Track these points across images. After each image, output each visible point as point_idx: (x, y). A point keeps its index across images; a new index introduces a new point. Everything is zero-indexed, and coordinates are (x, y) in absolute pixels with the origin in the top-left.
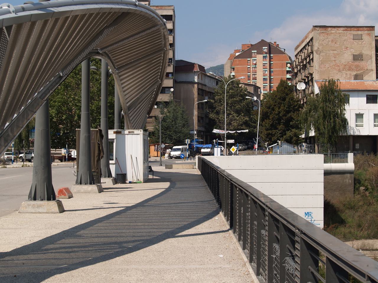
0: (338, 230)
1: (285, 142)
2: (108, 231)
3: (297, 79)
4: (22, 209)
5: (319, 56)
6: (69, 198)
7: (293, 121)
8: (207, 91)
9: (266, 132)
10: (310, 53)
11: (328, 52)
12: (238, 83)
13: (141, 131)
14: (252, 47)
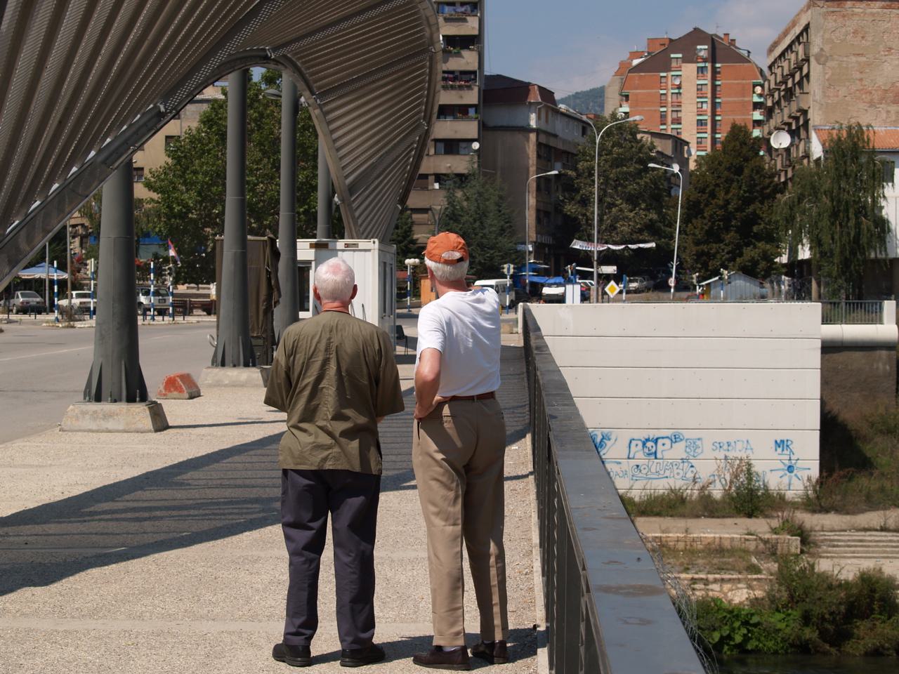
0: (853, 484)
1: (741, 273)
2: (250, 473)
3: (773, 123)
4: (67, 423)
5: (824, 69)
6: (191, 398)
7: (760, 224)
8: (559, 150)
9: (694, 249)
10: (803, 60)
11: (845, 59)
12: (634, 130)
13: (374, 242)
14: (673, 45)
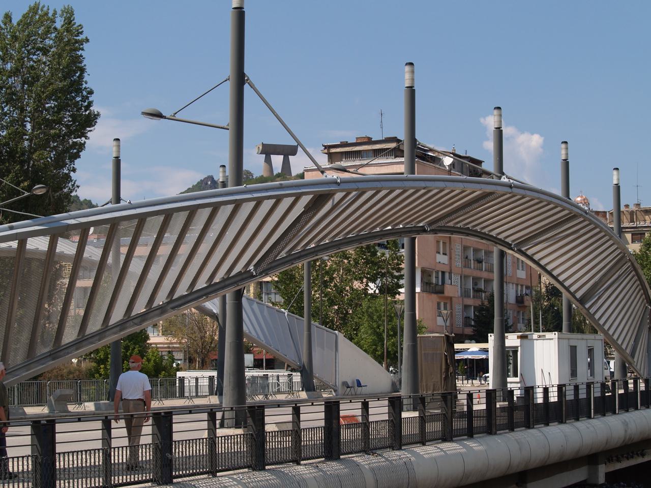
13: (555, 334)
